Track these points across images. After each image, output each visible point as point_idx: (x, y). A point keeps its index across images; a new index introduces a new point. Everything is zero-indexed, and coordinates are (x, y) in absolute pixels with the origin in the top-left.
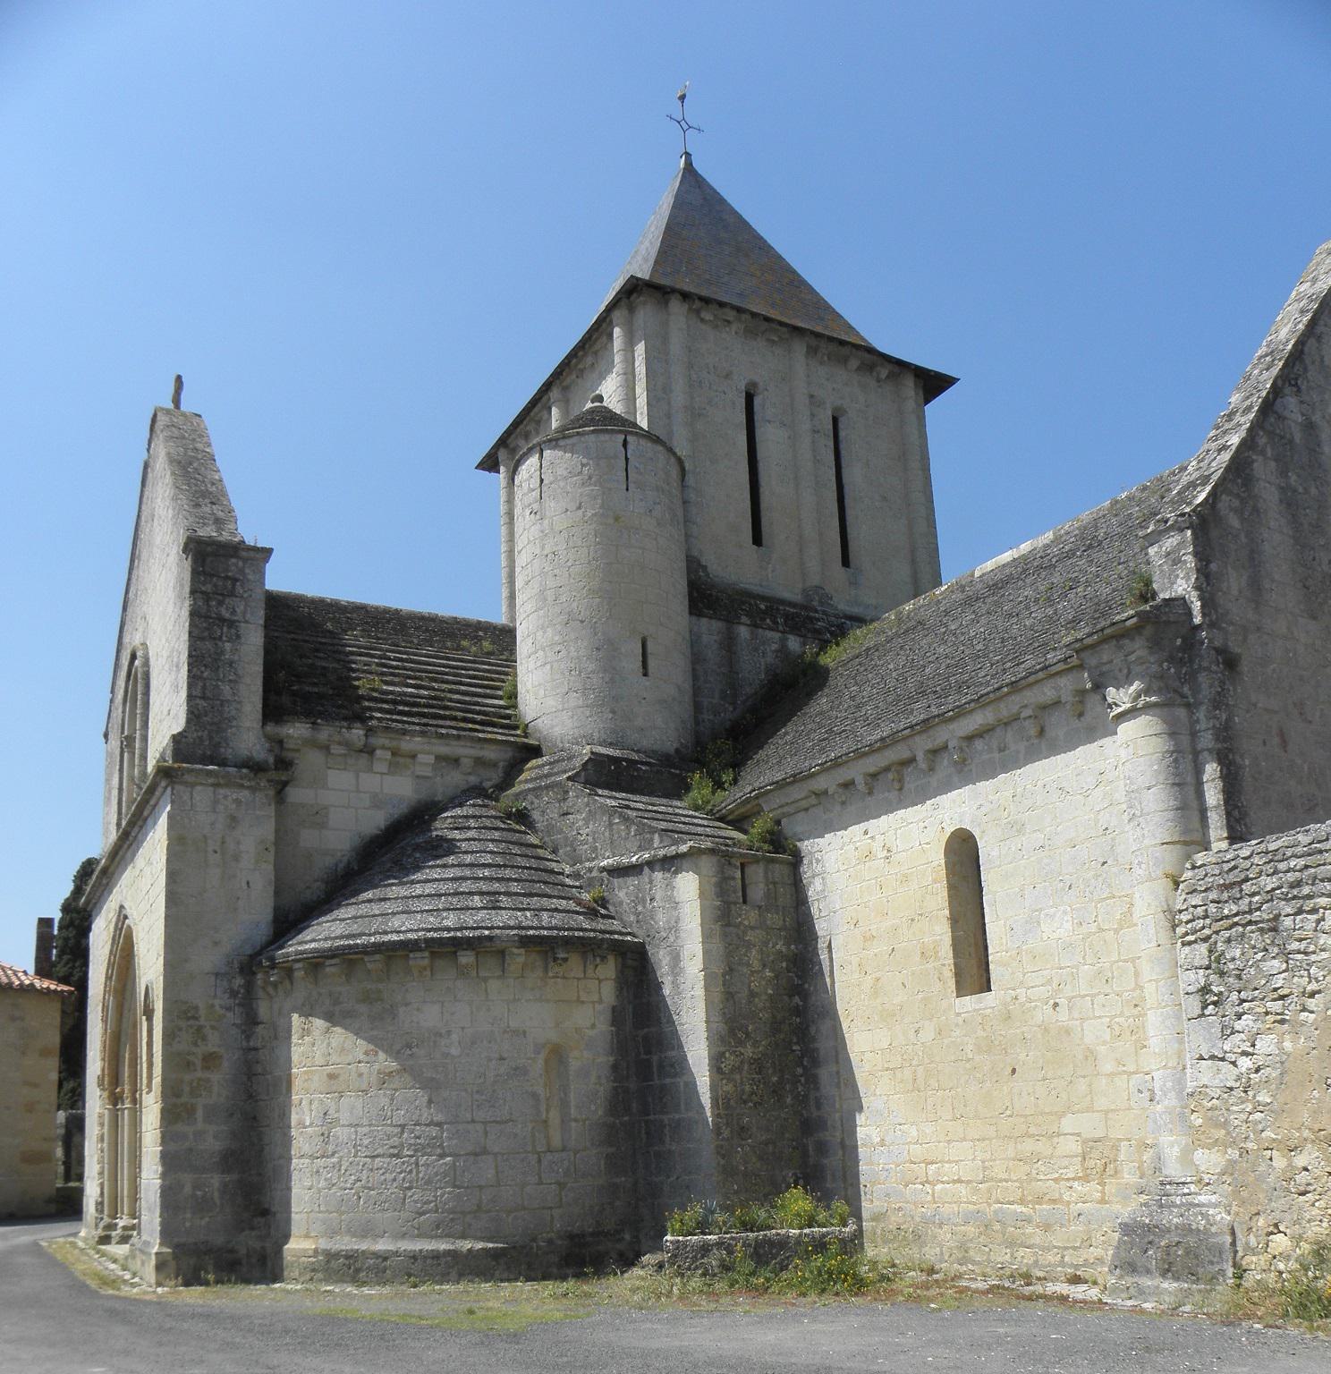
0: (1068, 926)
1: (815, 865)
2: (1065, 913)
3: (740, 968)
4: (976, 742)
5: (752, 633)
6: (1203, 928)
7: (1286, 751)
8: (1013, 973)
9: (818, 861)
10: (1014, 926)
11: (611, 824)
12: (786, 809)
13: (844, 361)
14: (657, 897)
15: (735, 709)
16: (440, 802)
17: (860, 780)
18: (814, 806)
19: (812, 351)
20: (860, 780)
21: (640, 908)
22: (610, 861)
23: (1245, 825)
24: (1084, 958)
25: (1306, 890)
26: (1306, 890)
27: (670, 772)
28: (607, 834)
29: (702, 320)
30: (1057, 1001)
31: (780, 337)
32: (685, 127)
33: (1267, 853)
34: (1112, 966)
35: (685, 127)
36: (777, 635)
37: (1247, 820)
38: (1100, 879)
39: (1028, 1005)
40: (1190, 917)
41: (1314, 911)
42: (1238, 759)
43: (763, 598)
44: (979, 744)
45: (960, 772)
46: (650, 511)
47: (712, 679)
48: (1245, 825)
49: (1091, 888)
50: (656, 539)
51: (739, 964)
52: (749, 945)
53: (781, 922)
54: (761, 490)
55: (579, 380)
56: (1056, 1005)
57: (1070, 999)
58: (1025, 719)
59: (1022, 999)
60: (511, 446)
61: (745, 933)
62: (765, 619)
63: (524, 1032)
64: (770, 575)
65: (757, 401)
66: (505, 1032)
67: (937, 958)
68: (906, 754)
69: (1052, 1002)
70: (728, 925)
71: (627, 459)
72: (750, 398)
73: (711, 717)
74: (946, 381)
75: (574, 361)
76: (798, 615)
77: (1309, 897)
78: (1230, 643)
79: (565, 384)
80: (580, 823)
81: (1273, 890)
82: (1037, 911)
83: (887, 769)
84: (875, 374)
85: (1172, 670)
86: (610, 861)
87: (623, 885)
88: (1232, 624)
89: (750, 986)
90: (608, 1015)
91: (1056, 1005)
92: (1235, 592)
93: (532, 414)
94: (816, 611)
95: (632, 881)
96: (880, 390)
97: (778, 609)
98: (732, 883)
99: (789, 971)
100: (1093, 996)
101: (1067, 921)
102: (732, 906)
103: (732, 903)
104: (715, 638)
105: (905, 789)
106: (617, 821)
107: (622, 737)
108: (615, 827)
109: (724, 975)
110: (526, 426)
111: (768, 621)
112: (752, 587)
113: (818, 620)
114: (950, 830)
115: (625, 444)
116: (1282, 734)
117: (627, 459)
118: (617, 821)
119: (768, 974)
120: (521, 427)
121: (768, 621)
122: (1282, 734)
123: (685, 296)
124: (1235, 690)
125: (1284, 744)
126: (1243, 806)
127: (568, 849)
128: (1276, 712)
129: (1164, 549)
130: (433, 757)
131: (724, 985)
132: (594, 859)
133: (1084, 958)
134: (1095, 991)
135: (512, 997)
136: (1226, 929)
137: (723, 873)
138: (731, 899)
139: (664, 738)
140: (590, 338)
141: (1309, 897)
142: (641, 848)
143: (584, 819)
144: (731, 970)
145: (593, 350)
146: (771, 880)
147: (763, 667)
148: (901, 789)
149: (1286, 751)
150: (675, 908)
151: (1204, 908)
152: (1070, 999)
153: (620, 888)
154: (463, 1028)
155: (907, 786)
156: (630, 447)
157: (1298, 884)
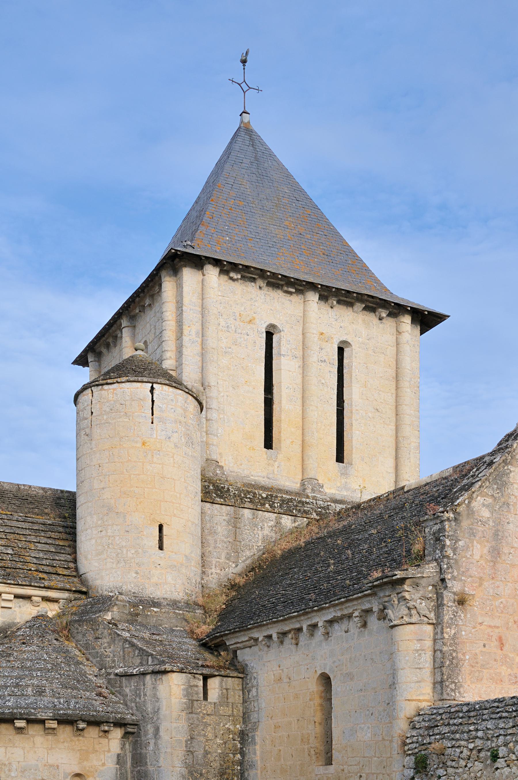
0: (369, 735)
1: (253, 680)
2: (368, 728)
3: (198, 737)
4: (335, 625)
5: (254, 514)
6: (416, 748)
7: (502, 650)
8: (343, 757)
9: (255, 678)
10: (345, 731)
11: (124, 648)
12: (238, 645)
13: (351, 305)
14: (148, 694)
15: (236, 566)
16: (18, 623)
17: (275, 636)
18: (254, 645)
19: (323, 298)
20: (275, 636)
21: (138, 700)
22: (121, 670)
23: (459, 692)
24: (375, 754)
25: (458, 736)
26: (458, 736)
27: (174, 613)
28: (121, 653)
29: (231, 279)
30: (362, 774)
31: (296, 289)
32: (245, 88)
33: (450, 713)
34: (387, 759)
35: (245, 88)
36: (273, 516)
37: (462, 690)
38: (386, 712)
39: (348, 775)
40: (411, 741)
41: (459, 747)
42: (460, 656)
43: (264, 488)
44: (336, 626)
45: (327, 639)
46: (169, 438)
47: (220, 546)
48: (459, 692)
49: (381, 716)
50: (173, 457)
51: (198, 736)
52: (206, 725)
53: (230, 712)
54: (274, 407)
55: (142, 314)
56: (361, 776)
57: (367, 774)
58: (355, 617)
59: (346, 771)
60: (97, 351)
61: (203, 718)
62: (264, 504)
63: (58, 766)
64: (276, 470)
65: (275, 338)
66: (45, 765)
67: (308, 743)
68: (297, 626)
69: (359, 775)
70: (191, 713)
71: (153, 401)
72: (269, 335)
73: (219, 571)
74: (441, 318)
75: (137, 299)
76: (291, 500)
77: (457, 740)
78: (466, 589)
79: (132, 314)
80: (106, 645)
81: (445, 733)
82: (356, 725)
83: (289, 631)
84: (377, 313)
85: (424, 604)
86: (121, 670)
87: (128, 685)
88: (471, 577)
89: (205, 748)
90: (115, 759)
91: (361, 776)
92: (477, 557)
93: (111, 331)
94: (308, 497)
95: (133, 682)
96: (381, 325)
97: (277, 497)
98: (196, 689)
99: (234, 740)
100: (378, 774)
101: (369, 732)
102: (195, 702)
103: (194, 700)
104: (224, 518)
105: (299, 644)
106: (127, 646)
107: (142, 589)
108: (126, 649)
109: (186, 741)
110: (107, 339)
111: (267, 506)
112: (261, 479)
113: (307, 503)
114: (319, 672)
115: (152, 389)
116: (500, 639)
117: (153, 401)
118: (127, 646)
119: (219, 741)
120: (104, 339)
121: (267, 506)
122: (500, 639)
123: (216, 262)
124: (465, 616)
125: (502, 645)
126: (459, 682)
127: (98, 659)
128: (498, 627)
129: (432, 530)
130: (13, 596)
131: (186, 747)
132: (113, 667)
133: (375, 754)
134: (378, 772)
135: (50, 746)
136: (424, 750)
137: (189, 682)
138: (194, 698)
139: (173, 590)
140: (147, 286)
141: (457, 740)
142: (141, 664)
143: (108, 643)
144: (192, 738)
145: (151, 293)
146: (224, 687)
147: (260, 538)
148: (297, 644)
149: (502, 650)
150: (157, 702)
151: (417, 738)
152: (367, 774)
153: (126, 687)
154: (19, 762)
155: (301, 643)
156: (156, 392)
157: (453, 733)
